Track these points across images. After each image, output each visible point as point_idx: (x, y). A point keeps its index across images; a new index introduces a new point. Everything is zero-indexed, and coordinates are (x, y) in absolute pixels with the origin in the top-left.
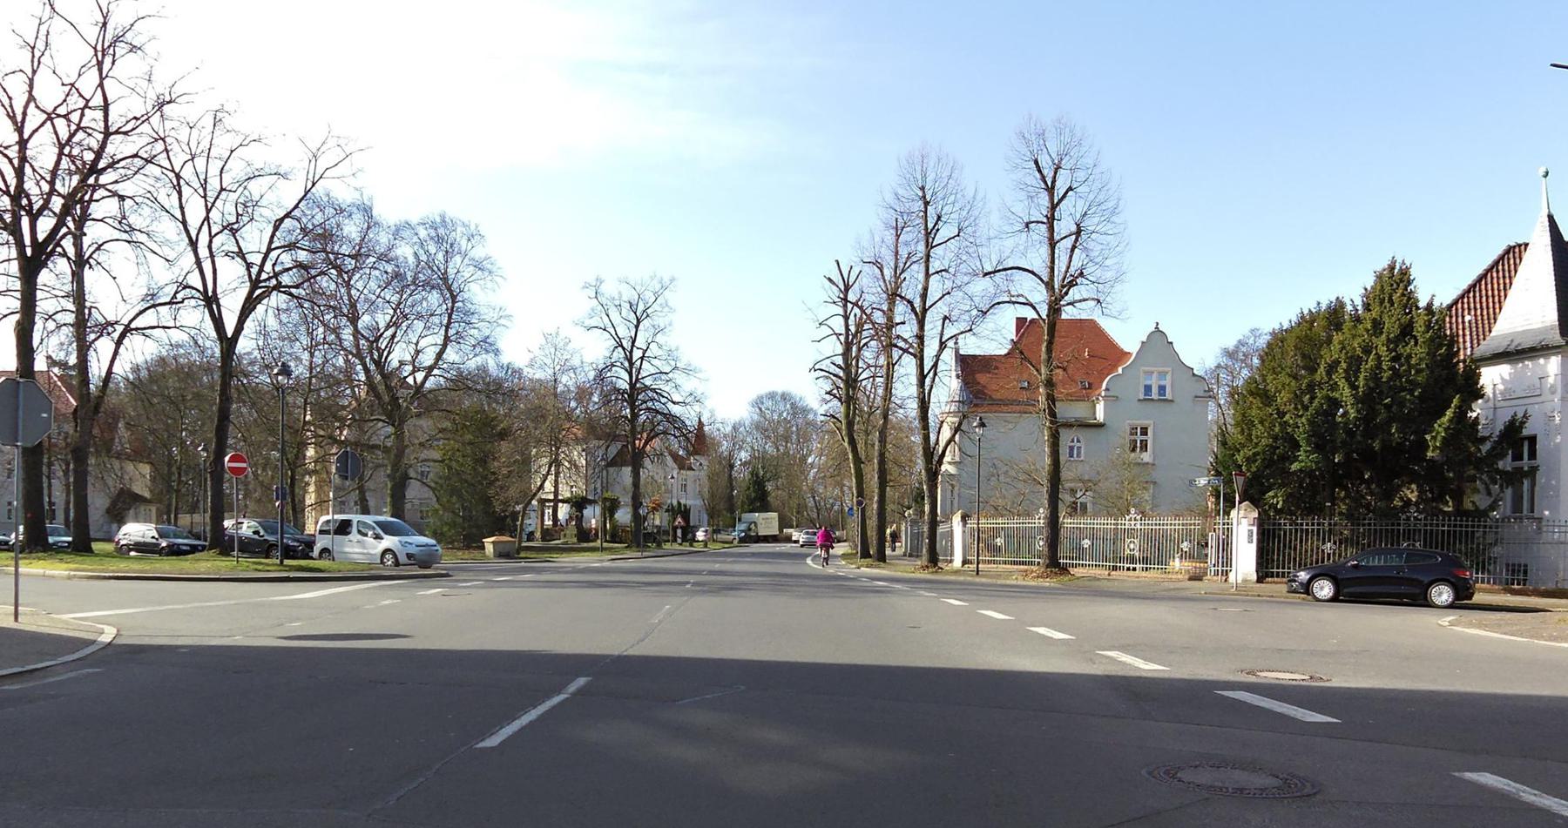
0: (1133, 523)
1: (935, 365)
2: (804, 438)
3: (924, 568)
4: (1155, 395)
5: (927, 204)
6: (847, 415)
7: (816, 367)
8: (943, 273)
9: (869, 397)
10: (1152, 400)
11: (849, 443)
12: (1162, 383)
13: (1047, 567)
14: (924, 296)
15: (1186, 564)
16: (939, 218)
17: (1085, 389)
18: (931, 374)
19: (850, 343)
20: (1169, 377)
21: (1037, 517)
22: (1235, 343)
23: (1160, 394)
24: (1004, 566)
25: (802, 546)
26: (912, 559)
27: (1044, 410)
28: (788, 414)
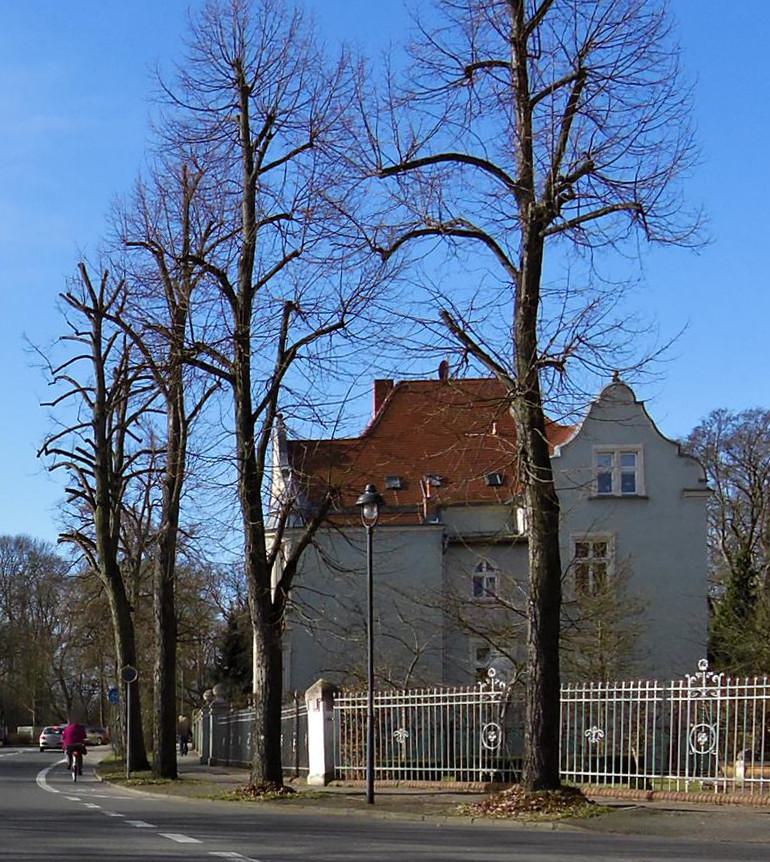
0: (703, 688)
1: (272, 396)
2: (47, 602)
3: (257, 790)
4: (616, 489)
5: (246, 92)
6: (104, 527)
7: (49, 448)
8: (282, 221)
9: (140, 523)
10: (613, 497)
11: (108, 574)
12: (628, 469)
13: (536, 787)
14: (247, 265)
15: (760, 771)
16: (270, 120)
17: (497, 485)
18: (263, 415)
19: (108, 404)
20: (639, 460)
21: (482, 686)
22: (690, 432)
23: (624, 488)
24: (411, 782)
25: (42, 749)
26: (219, 769)
27: (524, 452)
28: (25, 568)
